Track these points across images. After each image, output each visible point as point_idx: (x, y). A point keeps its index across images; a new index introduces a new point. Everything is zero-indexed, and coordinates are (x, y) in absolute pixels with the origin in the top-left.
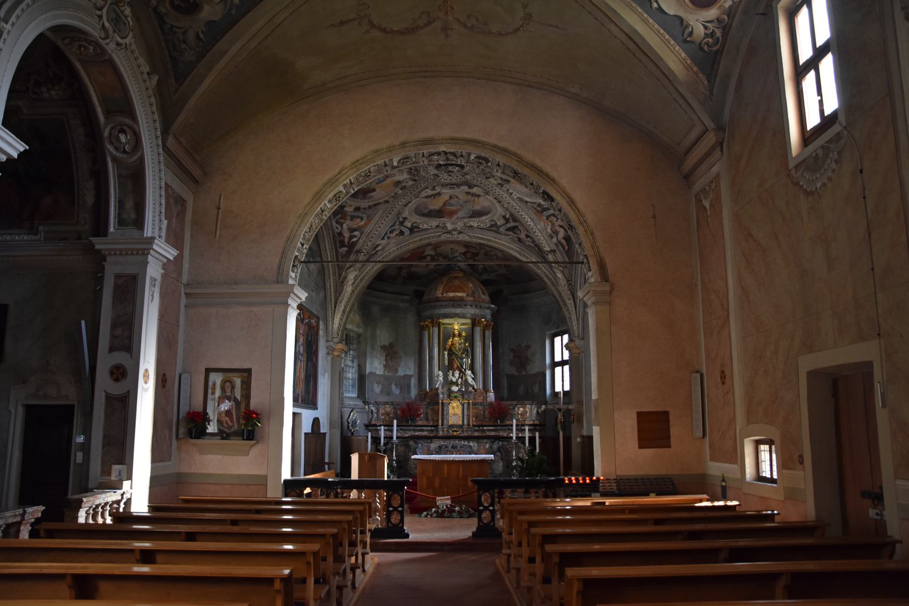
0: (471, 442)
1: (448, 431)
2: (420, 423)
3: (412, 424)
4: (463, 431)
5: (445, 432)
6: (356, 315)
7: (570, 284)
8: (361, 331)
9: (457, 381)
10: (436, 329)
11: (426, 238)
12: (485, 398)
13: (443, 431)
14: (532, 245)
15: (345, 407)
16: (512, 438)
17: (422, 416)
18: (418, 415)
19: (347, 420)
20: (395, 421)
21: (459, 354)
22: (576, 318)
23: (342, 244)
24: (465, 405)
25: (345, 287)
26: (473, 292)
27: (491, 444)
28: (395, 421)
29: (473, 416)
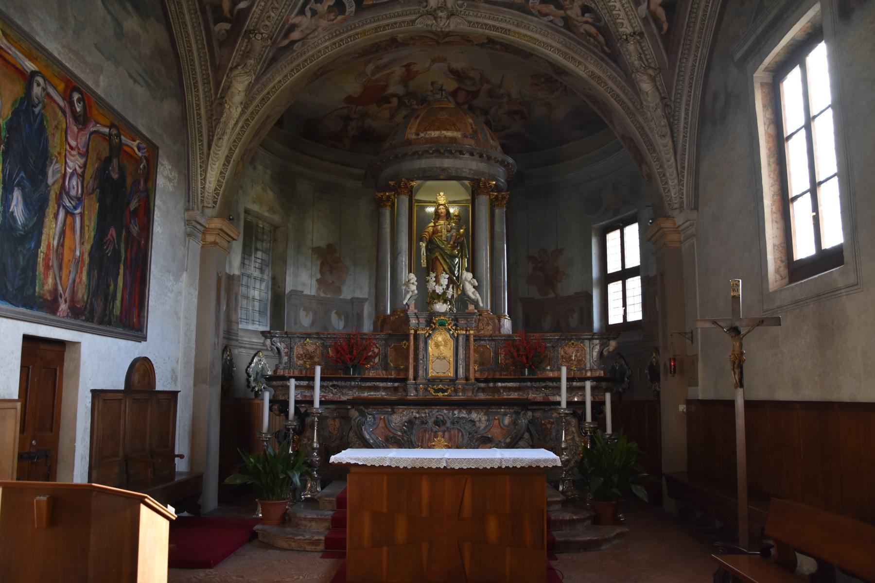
0: (473, 412)
1: (426, 390)
2: (372, 374)
3: (356, 376)
4: (456, 391)
5: (421, 393)
6: (269, 192)
7: (666, 105)
8: (276, 218)
9: (444, 293)
10: (405, 199)
11: (388, 25)
12: (499, 327)
13: (416, 390)
14: (592, 30)
15: (241, 347)
16: (559, 403)
17: (377, 360)
18: (368, 359)
19: (247, 370)
20: (318, 369)
21: (447, 248)
22: (675, 172)
23: (219, 17)
24: (461, 339)
25: (227, 106)
26: (475, 131)
27: (514, 416)
28: (318, 369)
29: (475, 362)
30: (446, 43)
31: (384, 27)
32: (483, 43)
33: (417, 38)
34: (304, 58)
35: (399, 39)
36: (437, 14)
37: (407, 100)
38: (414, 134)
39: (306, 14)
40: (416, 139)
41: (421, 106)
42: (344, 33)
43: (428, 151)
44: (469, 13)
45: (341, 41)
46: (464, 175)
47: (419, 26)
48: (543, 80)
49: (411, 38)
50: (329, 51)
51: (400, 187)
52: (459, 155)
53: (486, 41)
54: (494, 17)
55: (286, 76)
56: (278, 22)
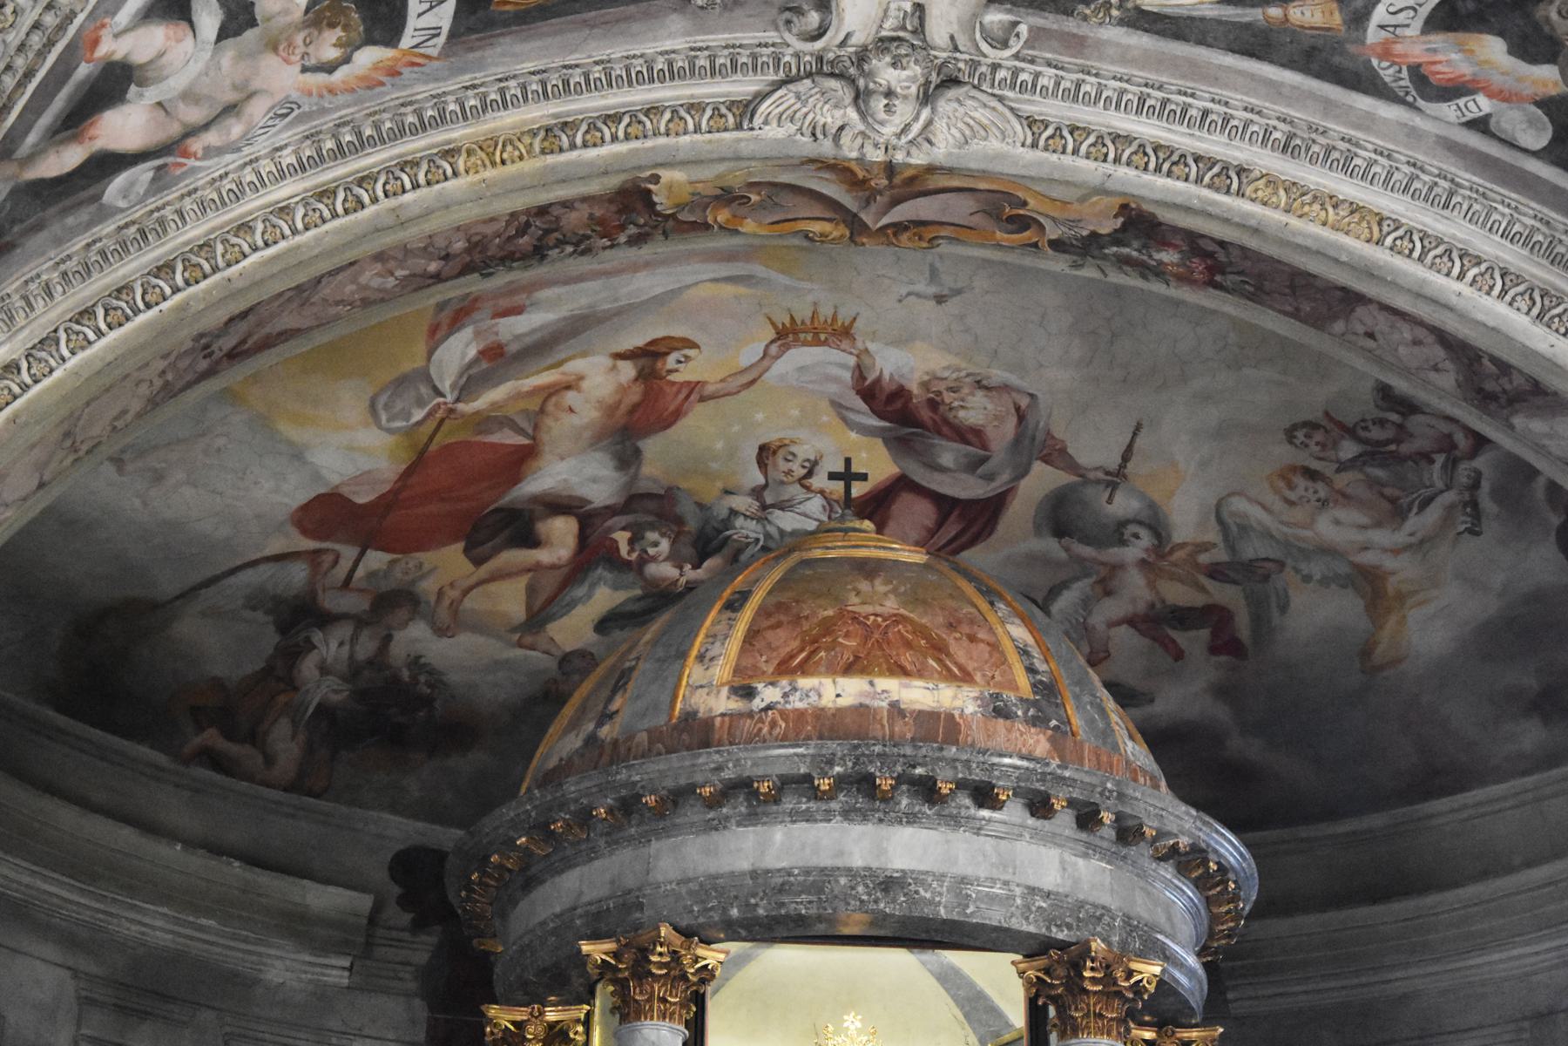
11: (613, 118)
26: (1047, 690)
30: (899, 228)
31: (592, 127)
32: (1094, 235)
33: (754, 198)
34: (156, 252)
35: (661, 199)
36: (869, 75)
37: (627, 535)
38: (725, 691)
39: (194, 19)
40: (733, 717)
41: (696, 566)
42: (380, 140)
43: (808, 778)
44: (1037, 75)
45: (360, 182)
46: (995, 917)
47: (773, 132)
48: (1349, 449)
49: (727, 197)
50: (295, 232)
51: (641, 971)
52: (972, 811)
53: (1107, 227)
54: (1165, 102)
55: (48, 341)
56: (36, 40)
